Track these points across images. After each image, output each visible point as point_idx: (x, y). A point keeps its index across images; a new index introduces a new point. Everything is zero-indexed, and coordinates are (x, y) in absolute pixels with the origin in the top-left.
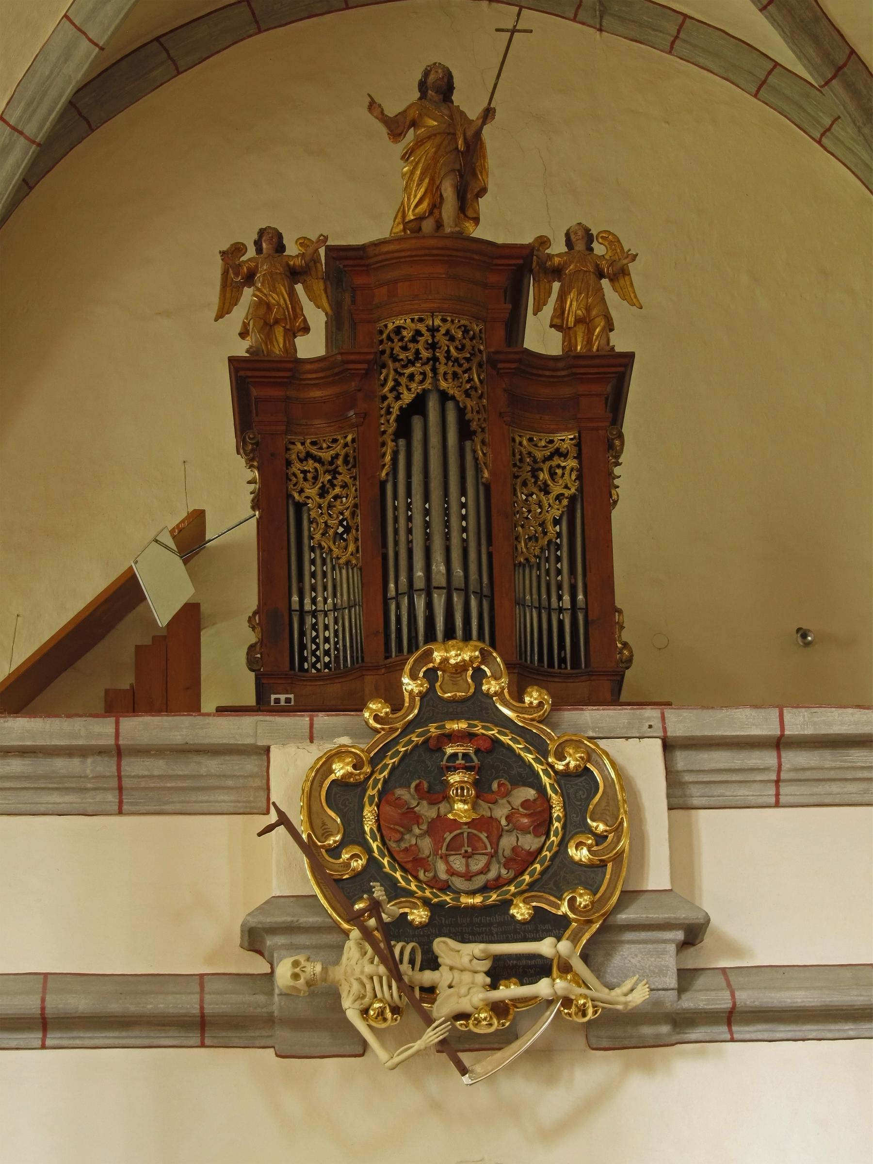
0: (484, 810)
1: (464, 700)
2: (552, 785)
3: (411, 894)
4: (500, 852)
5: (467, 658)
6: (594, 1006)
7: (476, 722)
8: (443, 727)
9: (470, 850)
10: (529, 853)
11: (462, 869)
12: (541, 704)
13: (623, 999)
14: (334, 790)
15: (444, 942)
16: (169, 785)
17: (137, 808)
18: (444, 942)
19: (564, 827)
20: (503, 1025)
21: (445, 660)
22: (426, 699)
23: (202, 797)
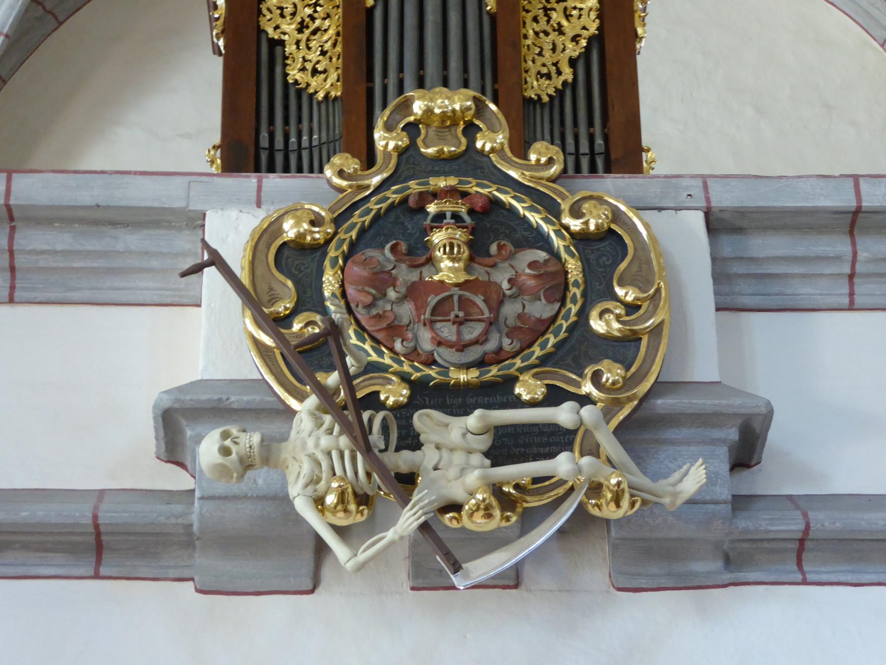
0: (480, 273)
1: (454, 158)
2: (567, 248)
3: (384, 368)
4: (501, 319)
5: (457, 107)
6: (632, 496)
7: (470, 179)
8: (427, 183)
9: (461, 314)
10: (540, 321)
11: (454, 338)
12: (550, 161)
13: (670, 489)
14: (286, 252)
15: (428, 416)
16: (75, 265)
17: (35, 294)
18: (428, 416)
19: (584, 295)
20: (508, 519)
21: (429, 111)
22: (405, 156)
23: (118, 282)
